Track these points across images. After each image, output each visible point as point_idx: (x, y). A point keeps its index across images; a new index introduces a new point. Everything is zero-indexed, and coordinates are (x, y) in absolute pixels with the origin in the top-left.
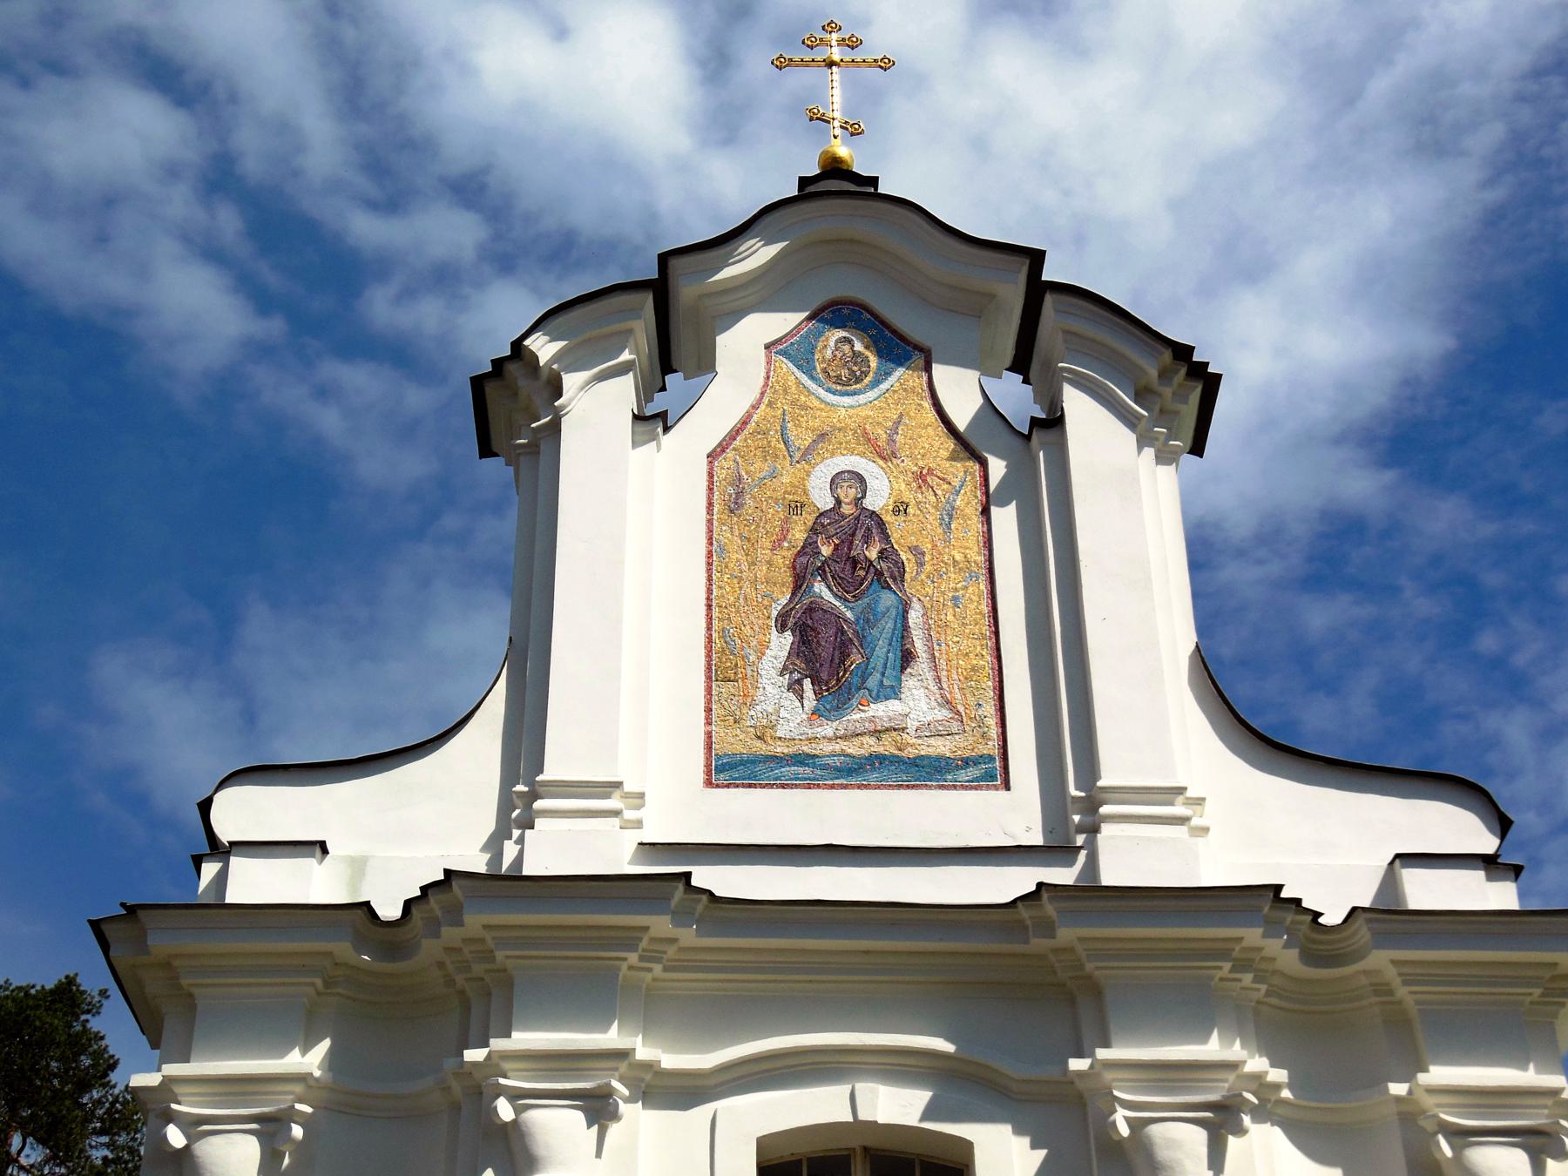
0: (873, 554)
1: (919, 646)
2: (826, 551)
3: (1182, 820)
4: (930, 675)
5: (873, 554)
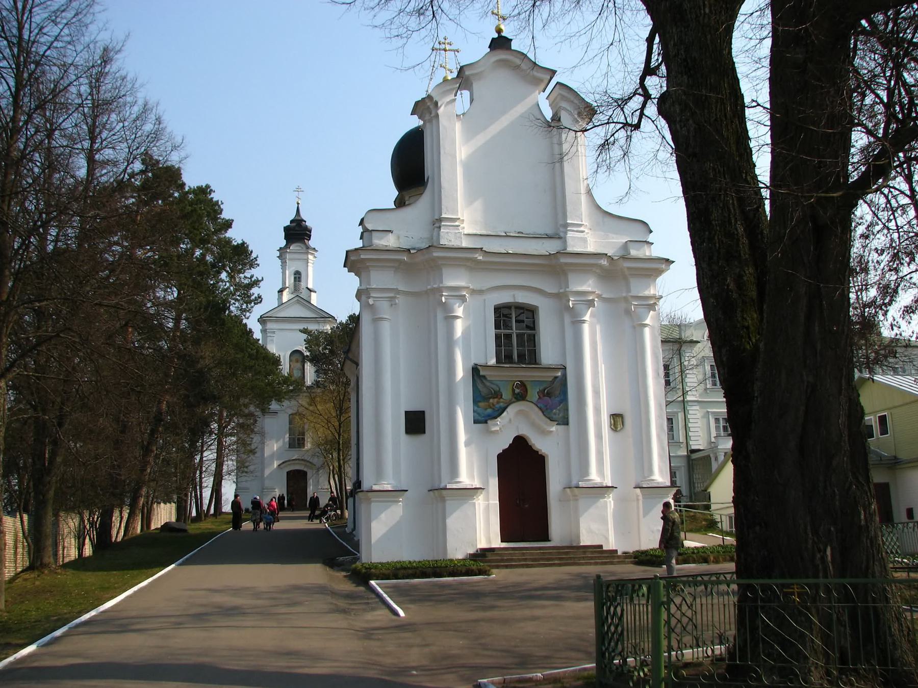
3: (583, 232)
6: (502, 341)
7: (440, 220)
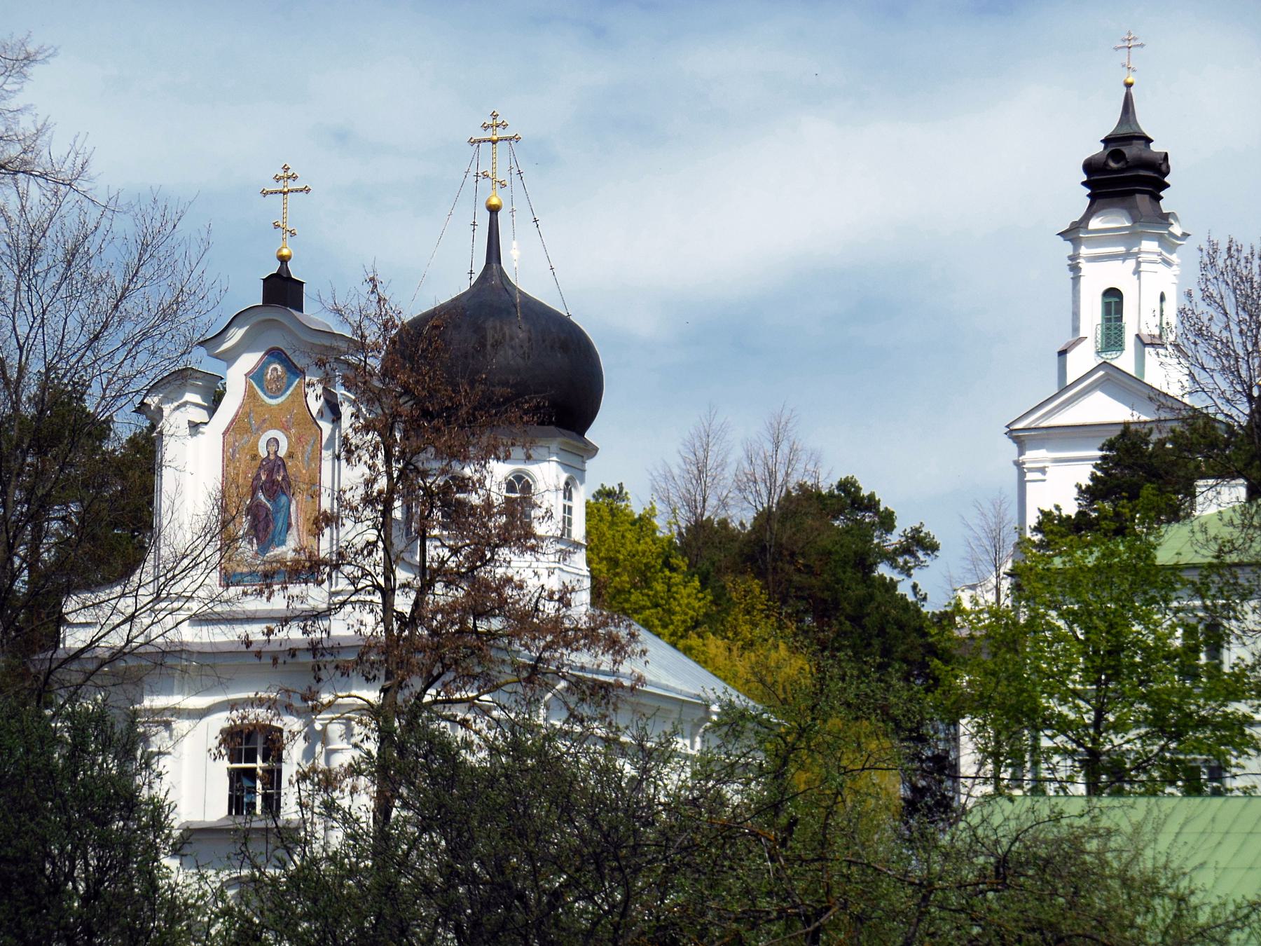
0: (280, 479)
1: (293, 521)
2: (263, 478)
4: (296, 537)
5: (280, 479)
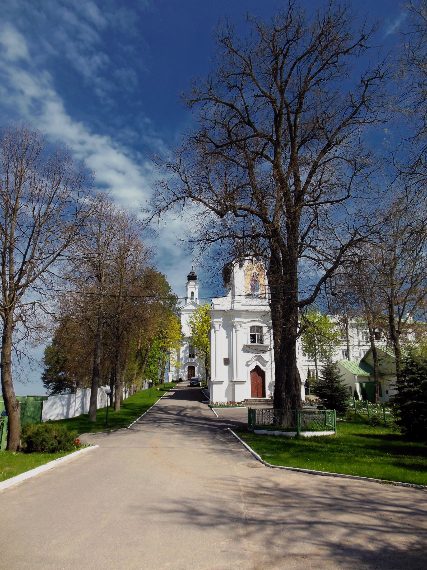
6: (253, 337)
7: (234, 301)
